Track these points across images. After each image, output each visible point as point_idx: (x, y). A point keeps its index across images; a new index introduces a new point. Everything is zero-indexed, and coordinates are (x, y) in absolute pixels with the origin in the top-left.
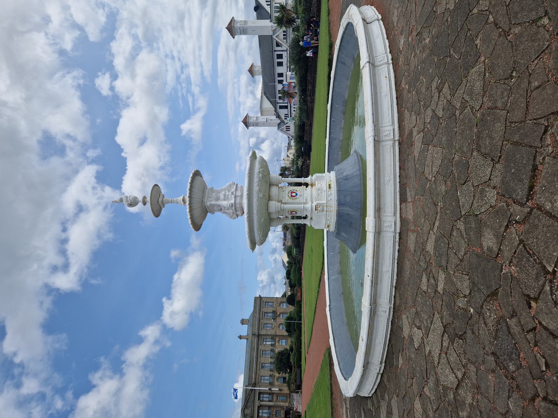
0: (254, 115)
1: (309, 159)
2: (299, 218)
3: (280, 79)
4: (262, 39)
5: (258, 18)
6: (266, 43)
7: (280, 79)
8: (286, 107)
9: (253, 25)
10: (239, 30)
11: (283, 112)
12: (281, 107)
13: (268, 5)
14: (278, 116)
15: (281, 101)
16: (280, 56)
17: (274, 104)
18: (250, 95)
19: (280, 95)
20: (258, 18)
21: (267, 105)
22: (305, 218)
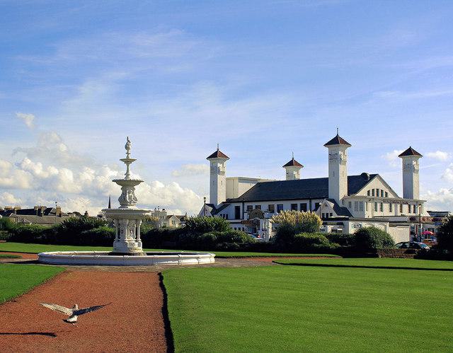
0: (230, 170)
1: (415, 257)
2: (119, 234)
3: (299, 207)
4: (324, 182)
5: (350, 179)
6: (318, 188)
7: (299, 207)
8: (237, 217)
9: (340, 172)
10: (334, 153)
11: (231, 210)
12: (237, 209)
13: (369, 192)
14: (225, 205)
15: (246, 209)
16: (304, 208)
17: (242, 200)
18: (26, 201)
19: (254, 208)
20: (350, 179)
21: (243, 189)
22: (119, 238)
